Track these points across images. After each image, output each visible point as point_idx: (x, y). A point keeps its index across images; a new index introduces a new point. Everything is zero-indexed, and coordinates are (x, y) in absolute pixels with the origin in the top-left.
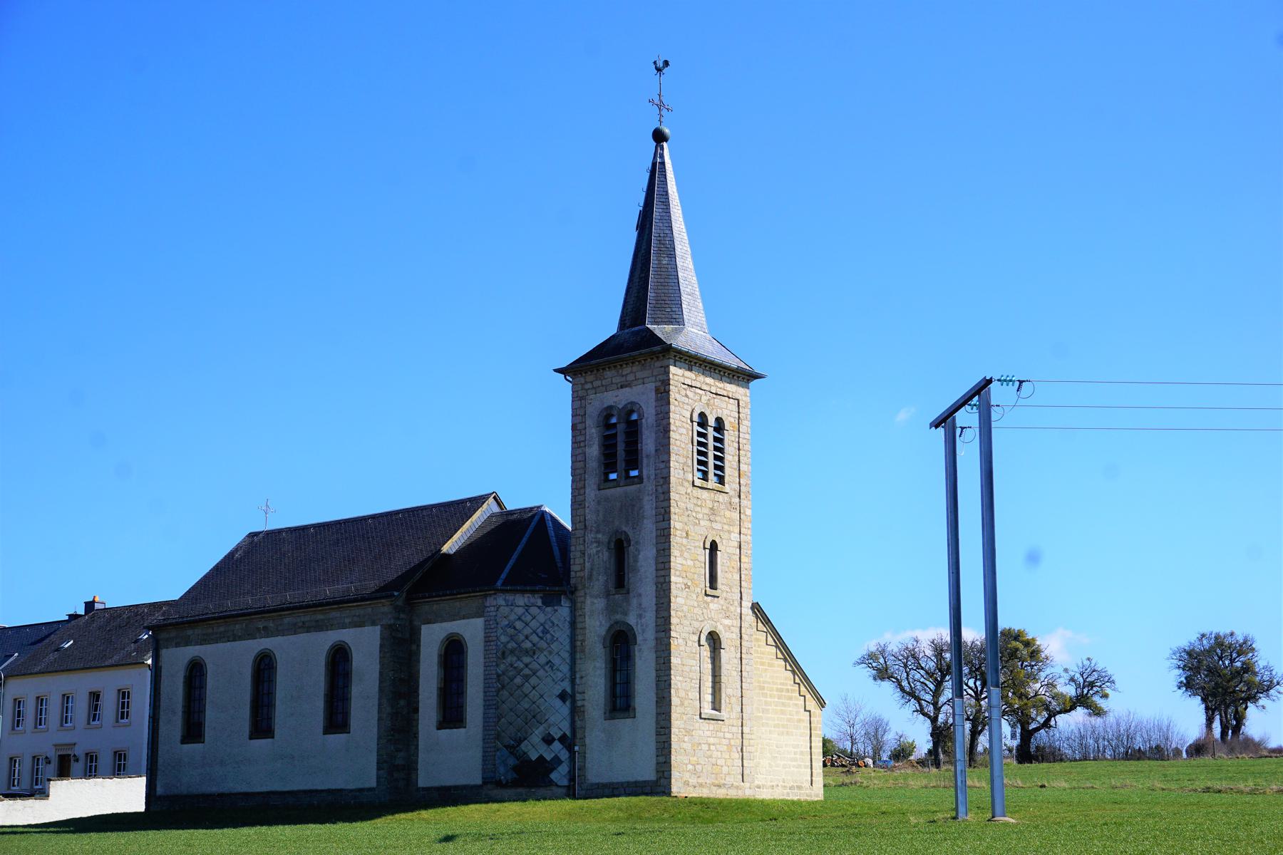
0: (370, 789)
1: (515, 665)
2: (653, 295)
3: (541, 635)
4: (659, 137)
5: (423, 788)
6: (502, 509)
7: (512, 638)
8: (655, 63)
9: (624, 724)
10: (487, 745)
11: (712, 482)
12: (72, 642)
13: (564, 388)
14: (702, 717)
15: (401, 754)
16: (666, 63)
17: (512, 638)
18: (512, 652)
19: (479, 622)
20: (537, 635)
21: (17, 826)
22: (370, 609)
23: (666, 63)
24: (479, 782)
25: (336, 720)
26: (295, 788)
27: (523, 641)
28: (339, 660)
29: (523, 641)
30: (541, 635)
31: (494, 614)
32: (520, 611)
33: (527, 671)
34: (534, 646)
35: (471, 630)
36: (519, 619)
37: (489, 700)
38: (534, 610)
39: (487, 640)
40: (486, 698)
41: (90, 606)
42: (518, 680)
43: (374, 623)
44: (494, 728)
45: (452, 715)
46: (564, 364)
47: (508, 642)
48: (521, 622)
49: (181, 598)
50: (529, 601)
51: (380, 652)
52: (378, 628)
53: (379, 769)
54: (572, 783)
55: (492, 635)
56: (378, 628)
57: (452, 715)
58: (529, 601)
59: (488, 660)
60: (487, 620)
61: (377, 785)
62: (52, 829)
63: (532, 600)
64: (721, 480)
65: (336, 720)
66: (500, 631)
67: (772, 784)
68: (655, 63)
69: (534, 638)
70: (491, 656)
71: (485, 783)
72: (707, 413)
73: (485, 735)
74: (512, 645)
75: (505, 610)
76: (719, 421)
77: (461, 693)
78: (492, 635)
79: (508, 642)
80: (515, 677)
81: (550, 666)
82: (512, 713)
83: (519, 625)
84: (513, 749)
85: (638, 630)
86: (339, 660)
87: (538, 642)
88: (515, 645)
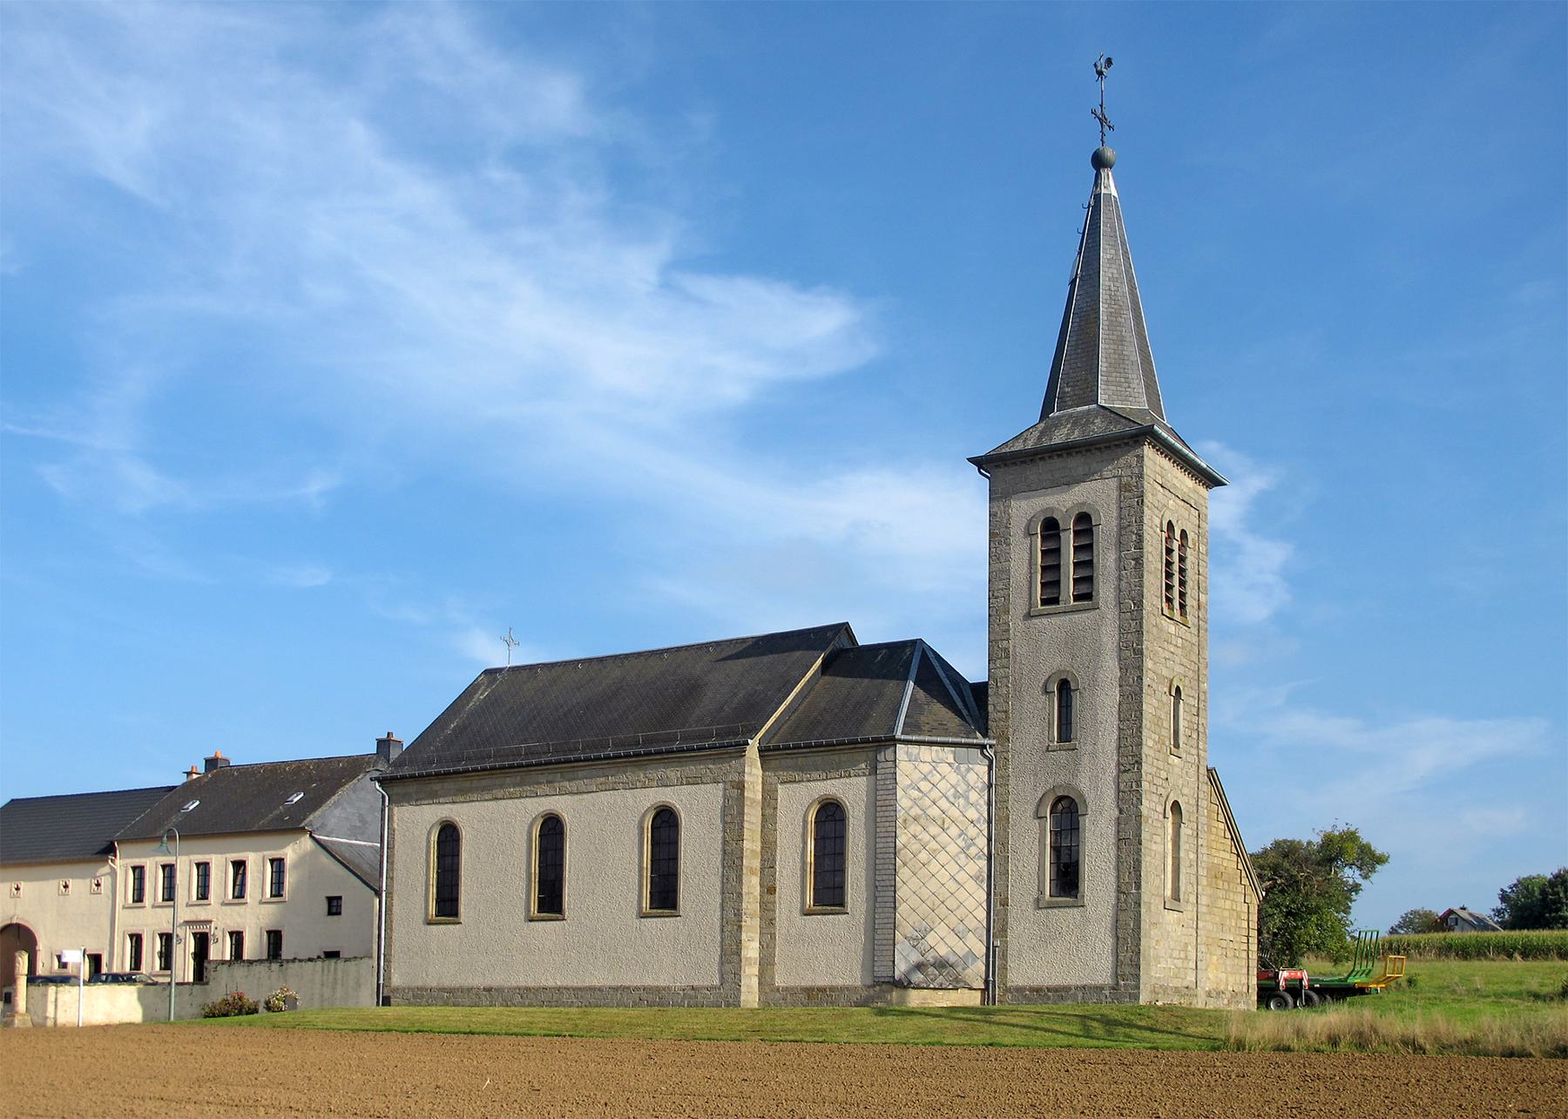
1: (920, 837)
2: (1105, 365)
4: (1099, 162)
6: (854, 644)
8: (1095, 65)
9: (1066, 917)
11: (1177, 614)
12: (198, 803)
13: (977, 486)
16: (1109, 62)
19: (862, 782)
21: (491, 994)
22: (519, 778)
23: (1109, 62)
27: (929, 807)
29: (929, 807)
30: (952, 799)
33: (933, 845)
36: (925, 778)
38: (944, 768)
41: (211, 763)
46: (981, 452)
47: (911, 808)
48: (928, 783)
49: (239, 768)
50: (938, 756)
54: (104, 978)
58: (938, 756)
62: (961, 1015)
63: (941, 754)
67: (1347, 1013)
68: (1095, 65)
69: (944, 803)
72: (1174, 523)
74: (915, 811)
77: (840, 870)
79: (911, 808)
80: (920, 852)
81: (963, 839)
83: (924, 786)
85: (1090, 797)
88: (920, 812)
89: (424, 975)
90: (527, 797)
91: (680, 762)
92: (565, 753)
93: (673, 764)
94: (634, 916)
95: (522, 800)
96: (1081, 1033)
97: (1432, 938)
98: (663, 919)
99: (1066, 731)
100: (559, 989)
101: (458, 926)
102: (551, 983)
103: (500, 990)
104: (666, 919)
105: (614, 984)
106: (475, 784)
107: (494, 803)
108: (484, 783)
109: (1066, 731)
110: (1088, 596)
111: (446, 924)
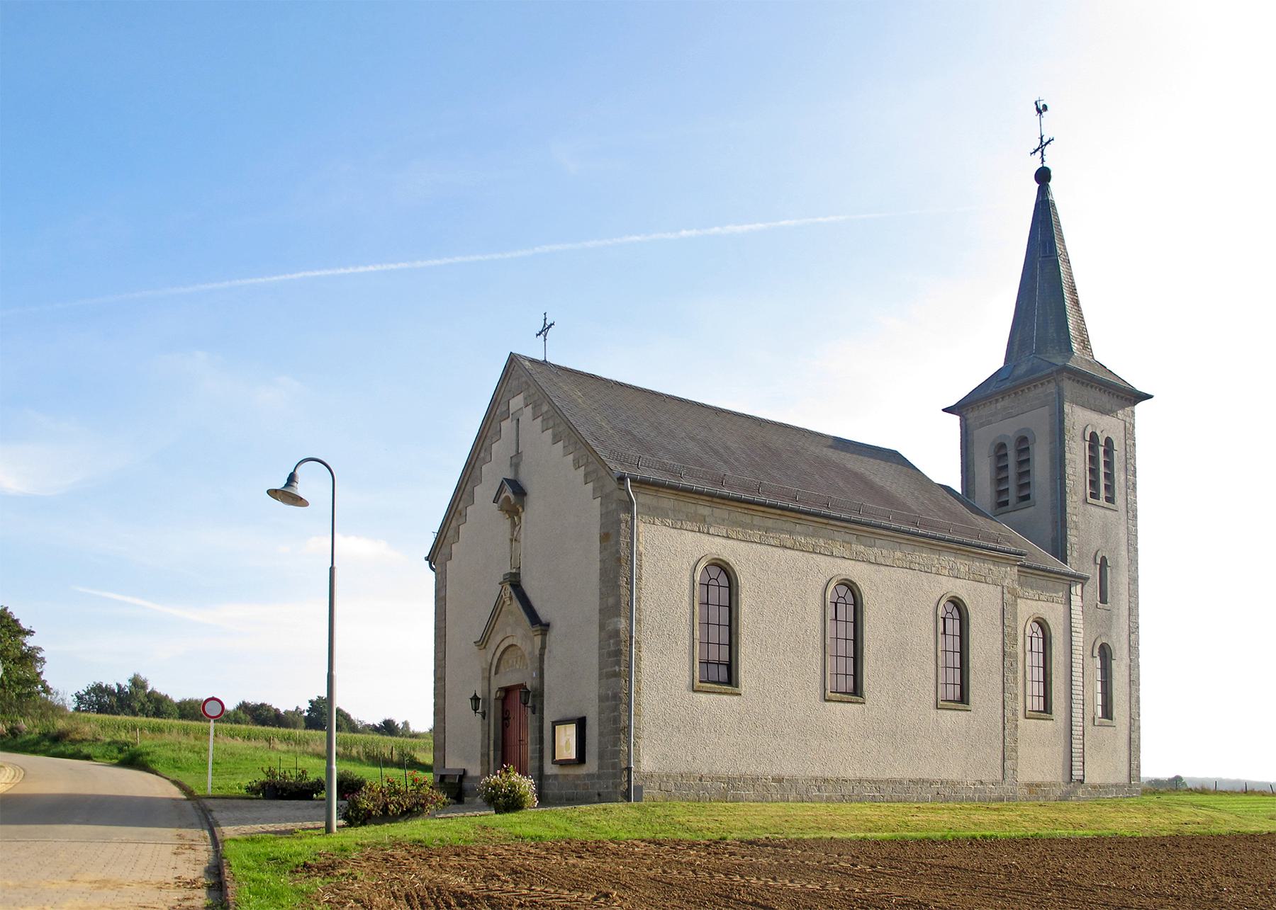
85: (1117, 646)
89: (690, 759)
90: (820, 553)
91: (968, 556)
92: (914, 524)
93: (964, 557)
94: (932, 708)
95: (814, 556)
96: (204, 800)
97: (151, 721)
98: (956, 712)
99: (1103, 600)
100: (860, 781)
101: (736, 698)
102: (850, 774)
103: (793, 781)
104: (960, 712)
105: (913, 777)
106: (757, 520)
107: (780, 551)
108: (769, 523)
109: (1103, 600)
110: (1027, 497)
111: (720, 693)
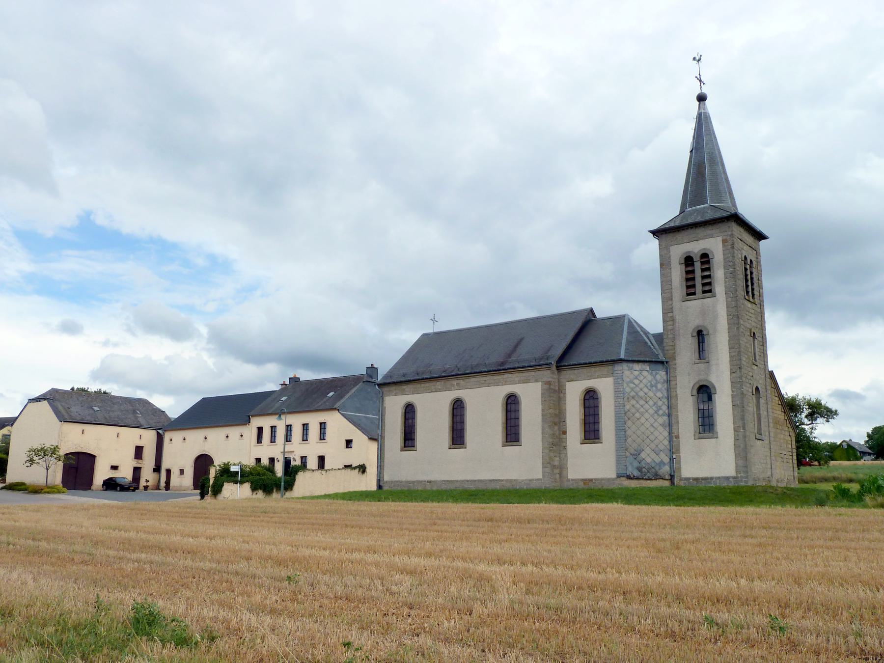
0: (539, 480)
3: (649, 388)
5: (573, 480)
7: (632, 389)
10: (619, 454)
14: (757, 438)
15: (557, 459)
17: (632, 389)
18: (633, 398)
20: (647, 388)
24: (614, 476)
25: (512, 434)
26: (482, 478)
28: (512, 403)
31: (621, 375)
32: (636, 373)
33: (642, 410)
34: (646, 394)
35: (604, 385)
37: (619, 458)
39: (616, 391)
40: (617, 426)
42: (637, 415)
43: (537, 381)
44: (624, 444)
45: (591, 433)
46: (655, 227)
51: (542, 397)
52: (540, 383)
53: (544, 467)
55: (620, 387)
56: (540, 383)
57: (591, 433)
59: (618, 403)
60: (616, 379)
61: (543, 477)
64: (753, 295)
65: (512, 434)
66: (625, 385)
69: (646, 390)
70: (620, 400)
71: (619, 476)
73: (618, 448)
75: (627, 373)
76: (751, 261)
78: (620, 387)
82: (635, 435)
83: (636, 382)
84: (636, 455)
86: (512, 403)
87: (649, 409)
